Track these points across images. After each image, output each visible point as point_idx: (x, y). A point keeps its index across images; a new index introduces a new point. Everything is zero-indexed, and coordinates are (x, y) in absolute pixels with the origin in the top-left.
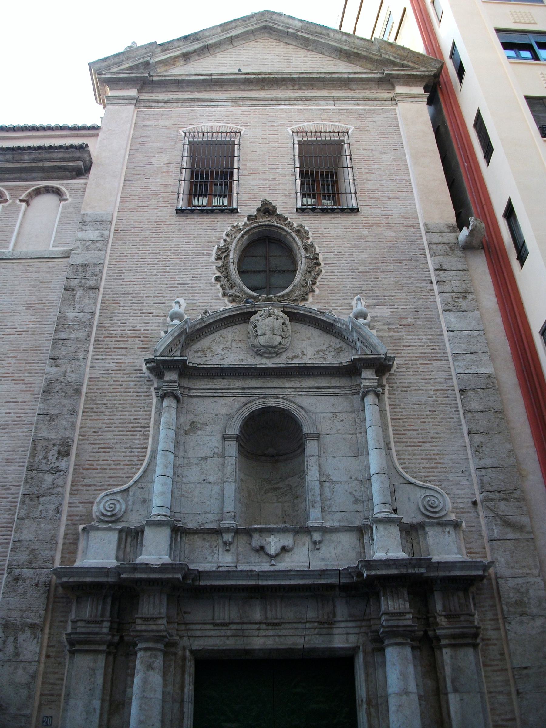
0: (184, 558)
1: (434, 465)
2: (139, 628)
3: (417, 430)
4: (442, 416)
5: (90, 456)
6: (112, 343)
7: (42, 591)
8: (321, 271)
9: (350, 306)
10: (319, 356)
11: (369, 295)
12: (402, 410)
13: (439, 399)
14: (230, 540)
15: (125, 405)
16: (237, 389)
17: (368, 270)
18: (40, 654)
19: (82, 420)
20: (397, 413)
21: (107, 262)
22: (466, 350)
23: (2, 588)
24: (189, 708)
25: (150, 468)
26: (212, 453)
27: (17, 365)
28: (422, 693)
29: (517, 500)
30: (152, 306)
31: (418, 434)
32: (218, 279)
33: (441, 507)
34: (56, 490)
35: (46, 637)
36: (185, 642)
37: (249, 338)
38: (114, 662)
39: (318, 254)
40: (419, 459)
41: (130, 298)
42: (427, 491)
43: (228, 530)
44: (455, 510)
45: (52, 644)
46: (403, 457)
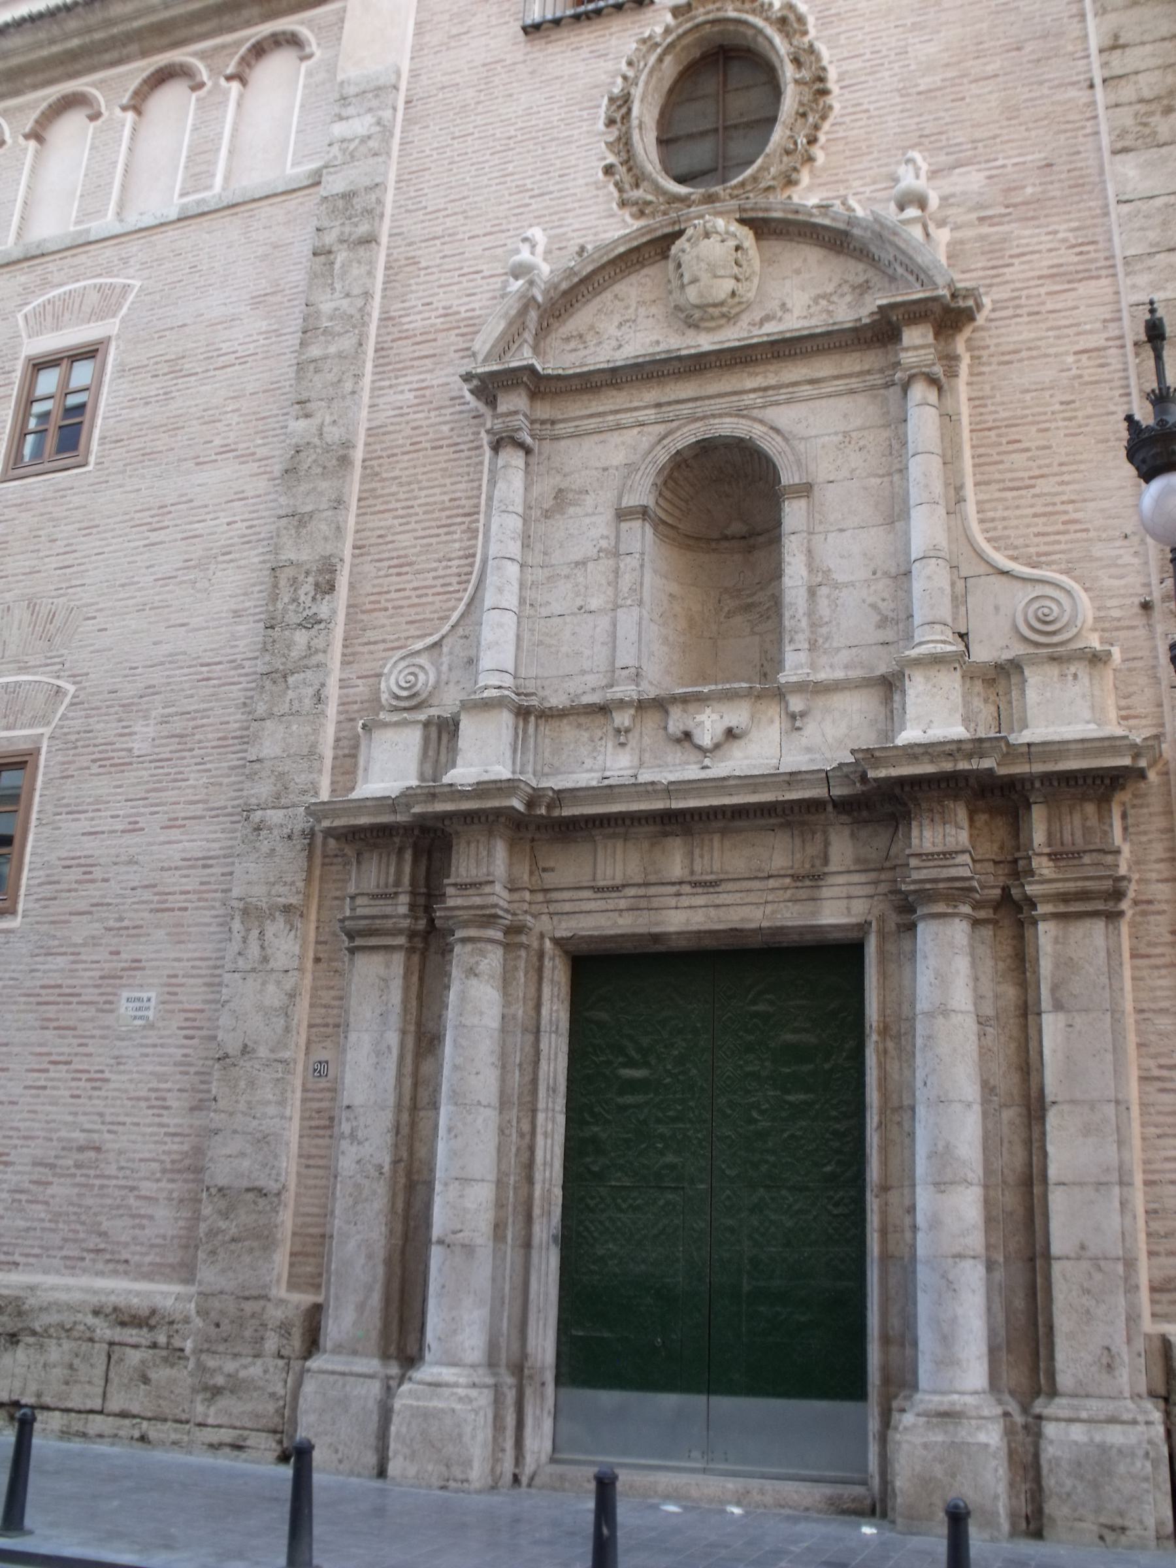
1: (1061, 527)
3: (1027, 450)
4: (1090, 411)
6: (405, 349)
7: (299, 847)
8: (831, 108)
10: (819, 308)
11: (939, 145)
12: (999, 408)
16: (646, 407)
17: (939, 84)
18: (301, 957)
20: (986, 417)
21: (392, 177)
22: (1158, 244)
28: (989, 1011)
31: (1029, 459)
32: (609, 170)
33: (1065, 619)
34: (314, 660)
35: (313, 926)
36: (544, 924)
40: (1027, 516)
41: (439, 247)
43: (622, 704)
44: (1102, 625)
46: (990, 514)
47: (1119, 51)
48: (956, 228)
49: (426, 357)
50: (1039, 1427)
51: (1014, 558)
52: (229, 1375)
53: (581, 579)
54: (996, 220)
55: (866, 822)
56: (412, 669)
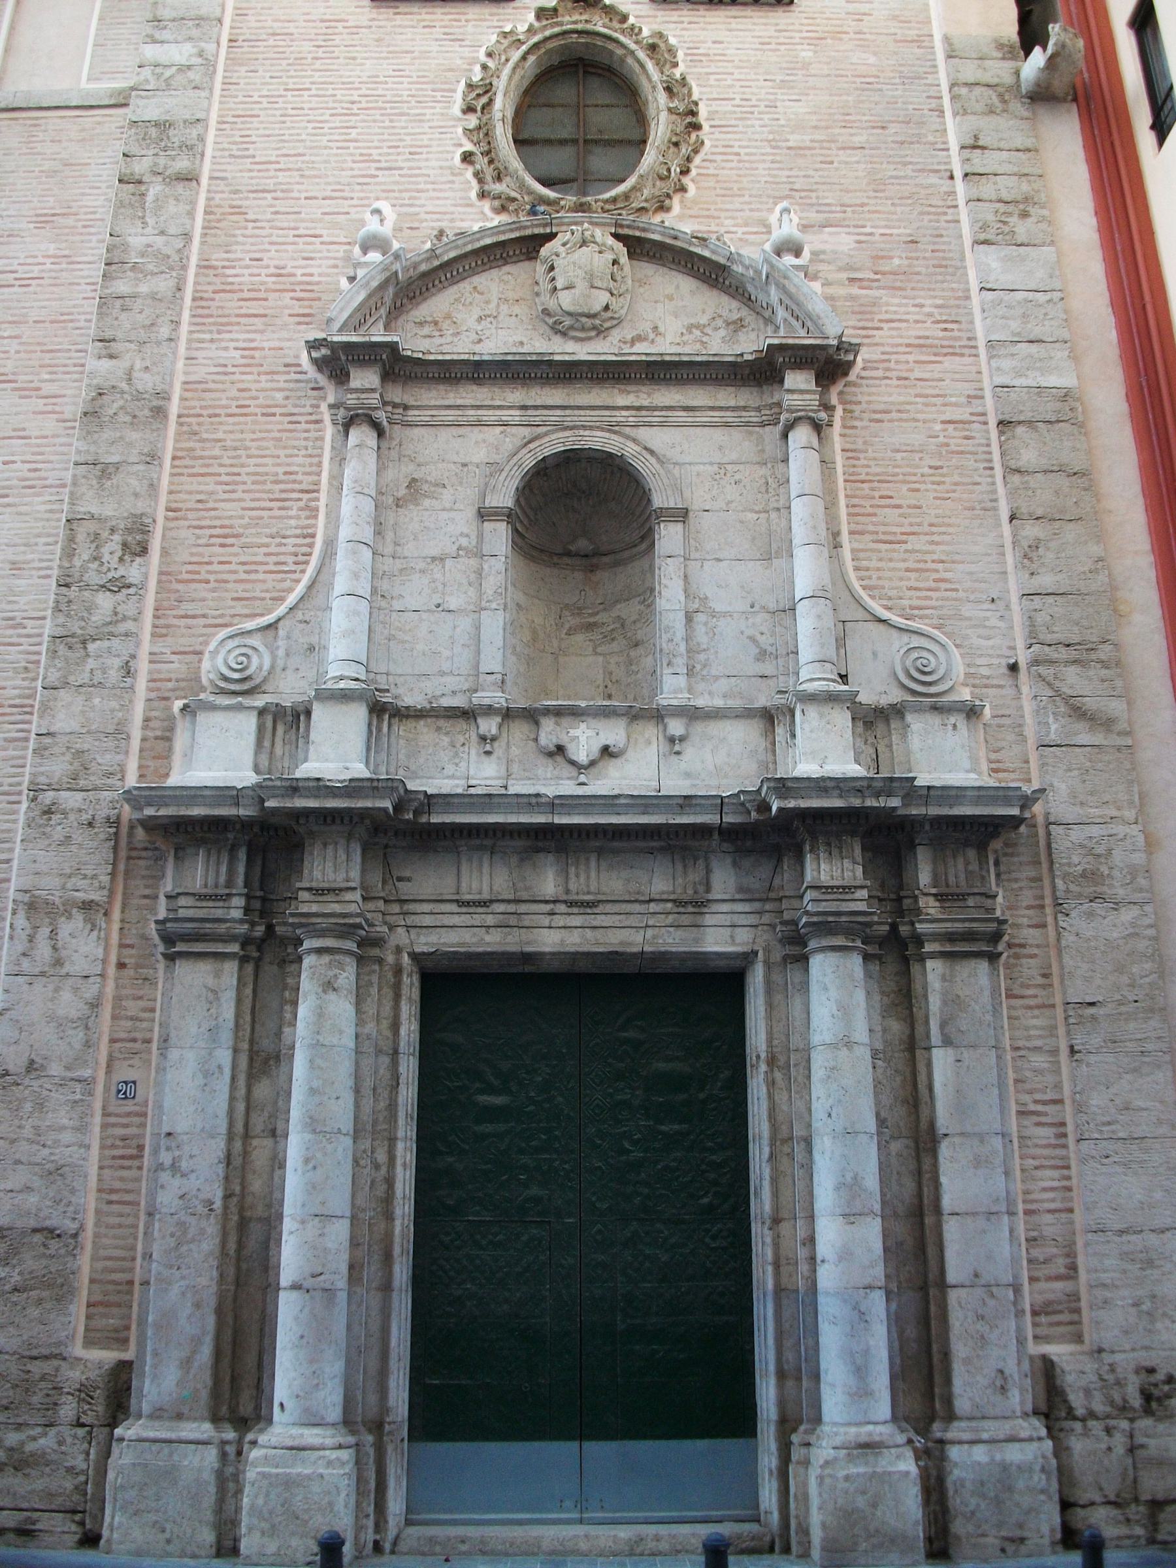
0: (397, 768)
2: (304, 909)
3: (899, 507)
4: (956, 478)
5: (192, 554)
7: (102, 836)
8: (703, 143)
9: (765, 226)
10: (692, 337)
12: (872, 463)
13: (952, 441)
14: (494, 731)
15: (264, 444)
16: (510, 408)
17: (808, 144)
18: (104, 961)
19: (172, 475)
20: (859, 470)
22: (1019, 334)
23: (20, 831)
24: (409, 1067)
25: (321, 578)
26: (455, 548)
27: (22, 355)
29: (1105, 664)
30: (321, 221)
32: (467, 158)
33: (941, 672)
34: (122, 628)
35: (116, 926)
36: (400, 937)
37: (537, 294)
38: (256, 976)
39: (696, 104)
42: (914, 637)
43: (489, 710)
44: (971, 681)
45: (128, 942)
46: (865, 563)
47: (979, 151)
48: (827, 284)
49: (255, 316)
50: (943, 1451)
51: (889, 609)
52: (12, 1449)
53: (438, 576)
54: (865, 284)
55: (749, 852)
56: (244, 650)
